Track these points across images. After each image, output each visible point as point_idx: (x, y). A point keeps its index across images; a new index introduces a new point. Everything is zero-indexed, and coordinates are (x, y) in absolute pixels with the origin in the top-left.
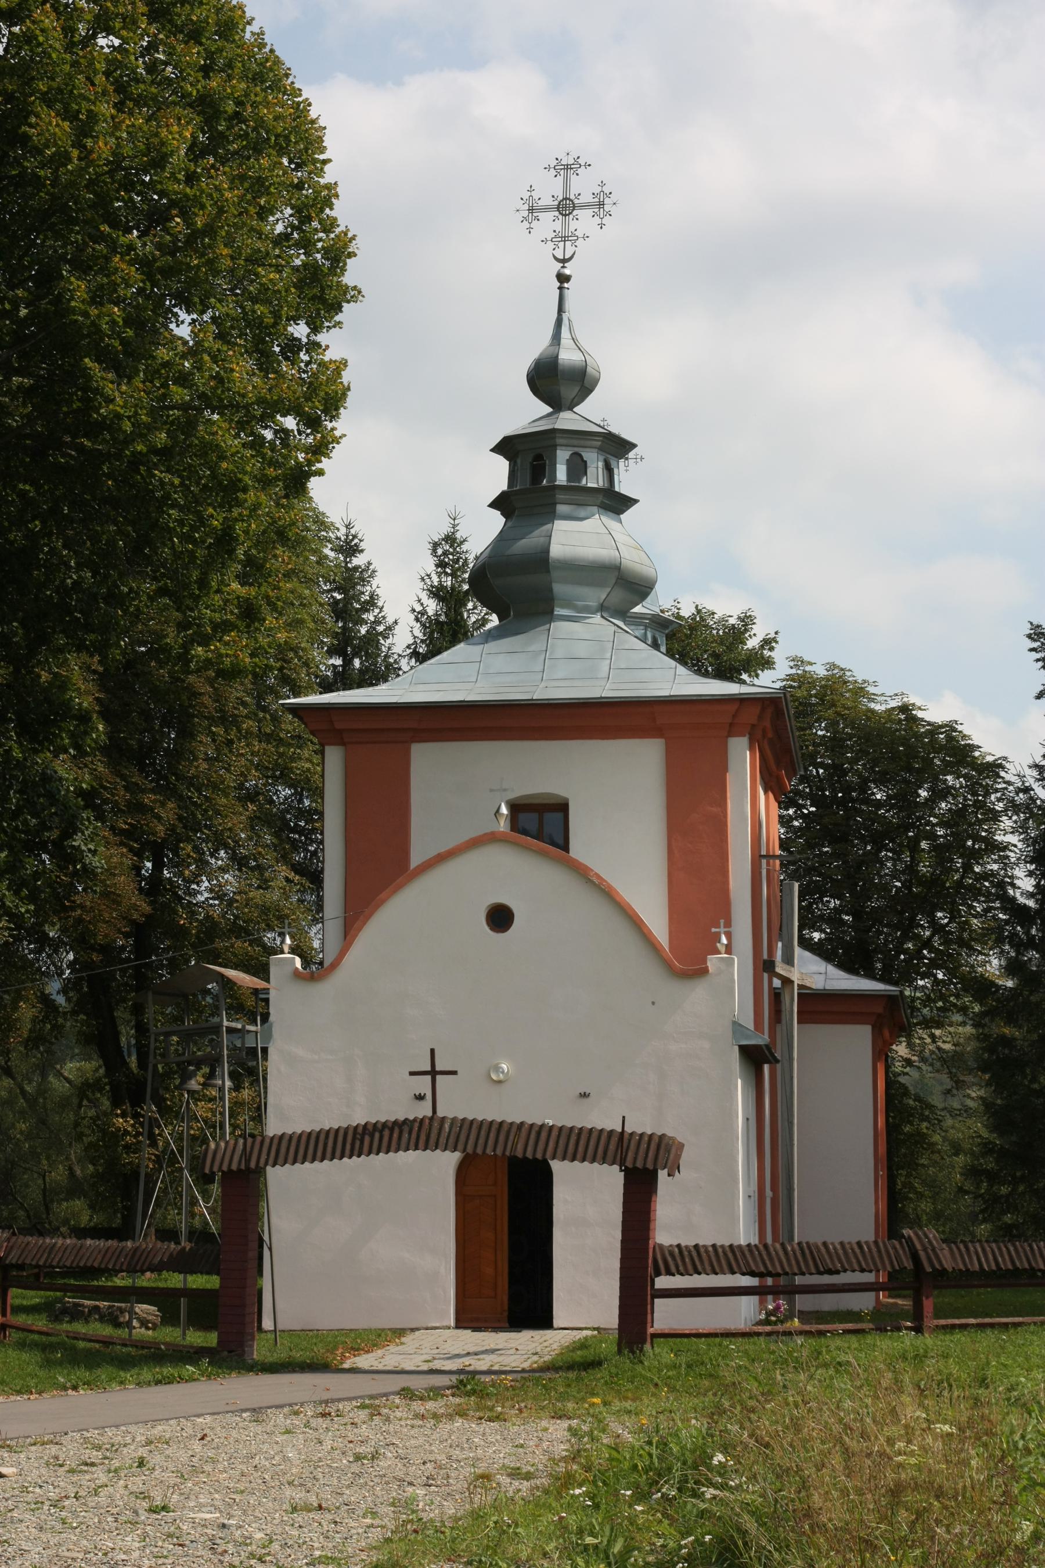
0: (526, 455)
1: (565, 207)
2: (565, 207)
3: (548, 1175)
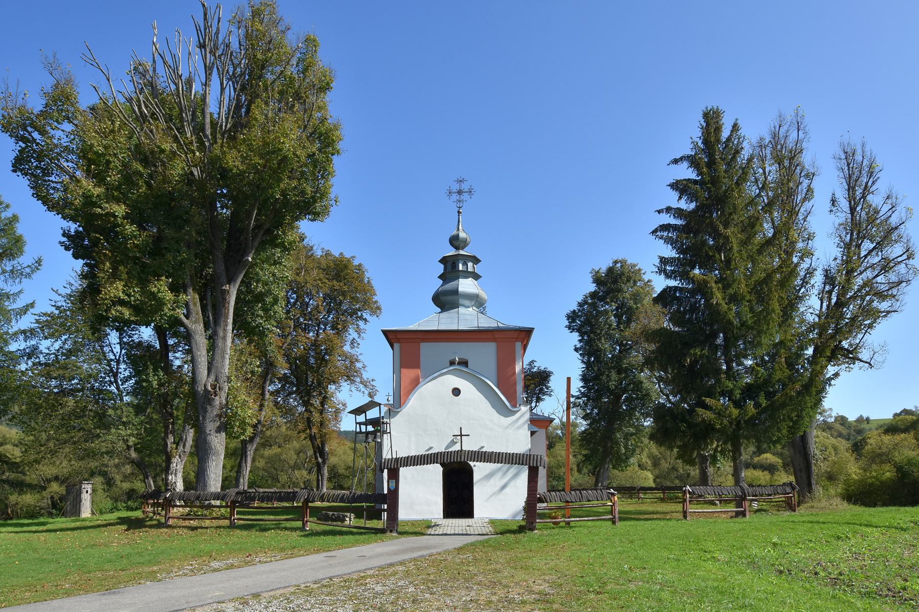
1: (460, 192)
2: (460, 192)
3: (470, 472)
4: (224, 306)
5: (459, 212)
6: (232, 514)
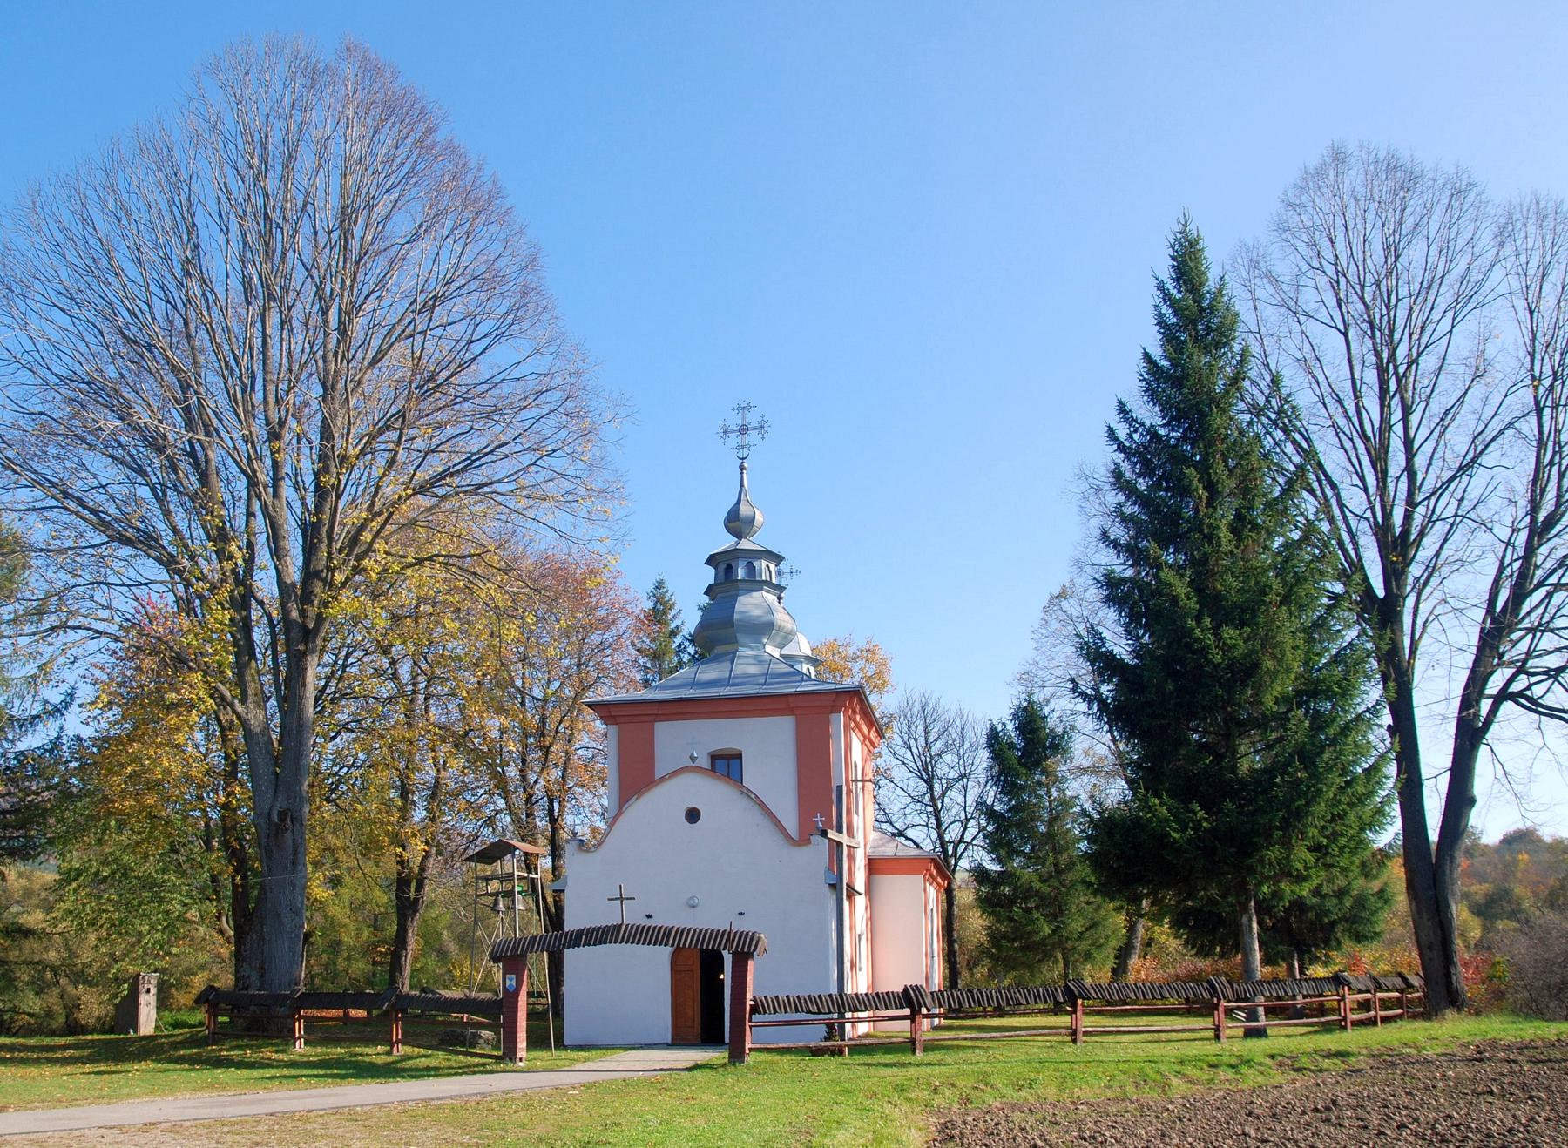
0: (723, 563)
1: (743, 430)
2: (743, 430)
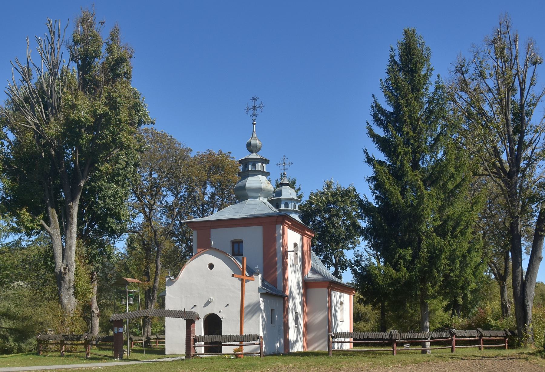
1: (254, 108)
2: (254, 108)
4: (70, 217)
5: (253, 124)
6: (62, 348)
